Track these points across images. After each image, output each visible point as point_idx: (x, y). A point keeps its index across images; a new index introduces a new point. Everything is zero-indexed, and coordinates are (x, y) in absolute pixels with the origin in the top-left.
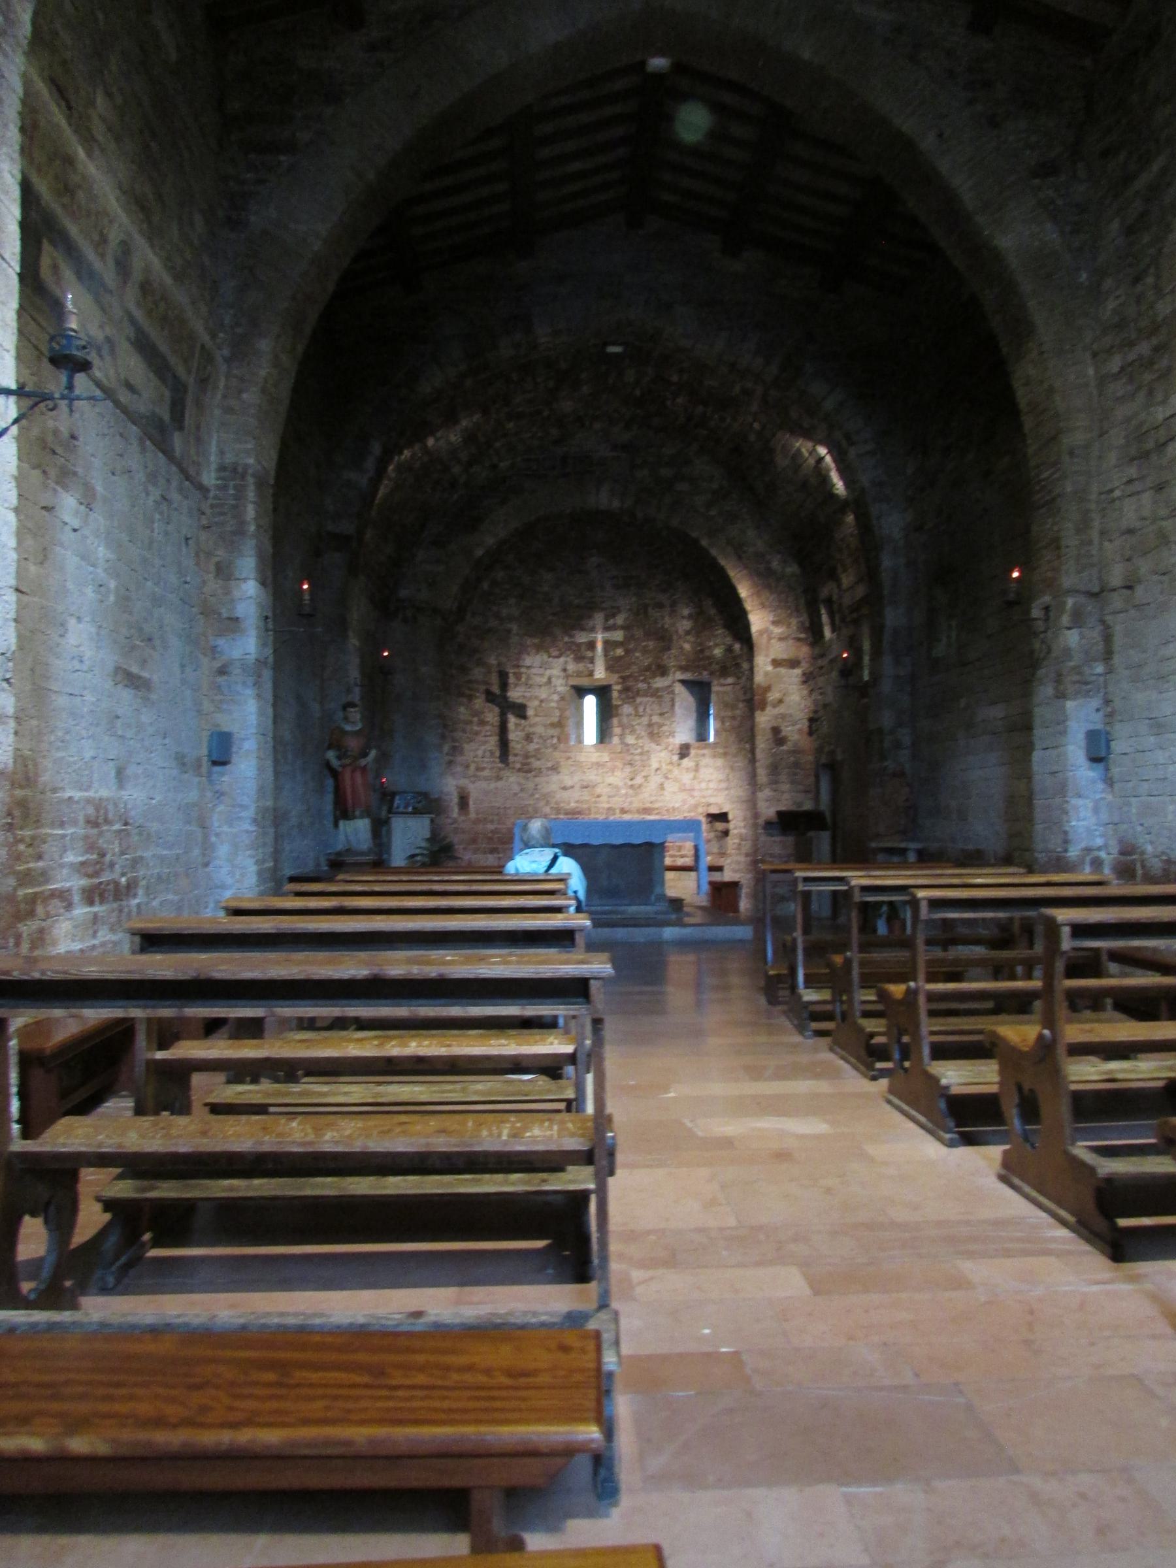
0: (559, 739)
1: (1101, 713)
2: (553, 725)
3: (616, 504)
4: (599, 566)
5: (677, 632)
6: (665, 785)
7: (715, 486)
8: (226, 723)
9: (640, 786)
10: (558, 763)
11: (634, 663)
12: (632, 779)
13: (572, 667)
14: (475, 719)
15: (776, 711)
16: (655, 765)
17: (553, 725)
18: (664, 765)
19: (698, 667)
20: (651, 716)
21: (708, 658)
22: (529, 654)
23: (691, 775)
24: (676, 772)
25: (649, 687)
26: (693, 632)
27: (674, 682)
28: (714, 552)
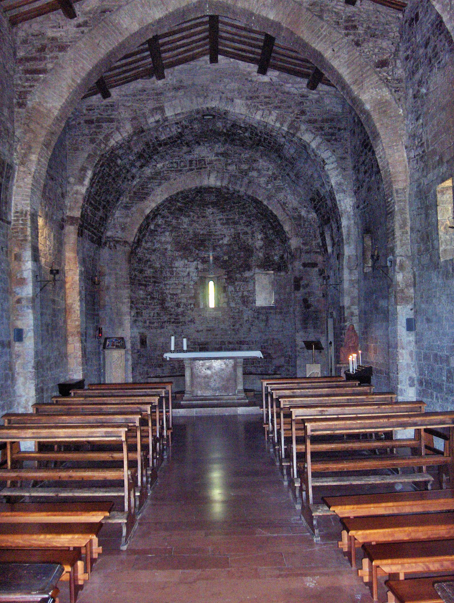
0: (194, 305)
1: (413, 311)
3: (219, 184)
4: (213, 213)
5: (255, 247)
7: (270, 173)
8: (19, 324)
13: (200, 267)
14: (149, 297)
16: (246, 318)
17: (191, 298)
22: (177, 260)
25: (242, 276)
28: (270, 208)
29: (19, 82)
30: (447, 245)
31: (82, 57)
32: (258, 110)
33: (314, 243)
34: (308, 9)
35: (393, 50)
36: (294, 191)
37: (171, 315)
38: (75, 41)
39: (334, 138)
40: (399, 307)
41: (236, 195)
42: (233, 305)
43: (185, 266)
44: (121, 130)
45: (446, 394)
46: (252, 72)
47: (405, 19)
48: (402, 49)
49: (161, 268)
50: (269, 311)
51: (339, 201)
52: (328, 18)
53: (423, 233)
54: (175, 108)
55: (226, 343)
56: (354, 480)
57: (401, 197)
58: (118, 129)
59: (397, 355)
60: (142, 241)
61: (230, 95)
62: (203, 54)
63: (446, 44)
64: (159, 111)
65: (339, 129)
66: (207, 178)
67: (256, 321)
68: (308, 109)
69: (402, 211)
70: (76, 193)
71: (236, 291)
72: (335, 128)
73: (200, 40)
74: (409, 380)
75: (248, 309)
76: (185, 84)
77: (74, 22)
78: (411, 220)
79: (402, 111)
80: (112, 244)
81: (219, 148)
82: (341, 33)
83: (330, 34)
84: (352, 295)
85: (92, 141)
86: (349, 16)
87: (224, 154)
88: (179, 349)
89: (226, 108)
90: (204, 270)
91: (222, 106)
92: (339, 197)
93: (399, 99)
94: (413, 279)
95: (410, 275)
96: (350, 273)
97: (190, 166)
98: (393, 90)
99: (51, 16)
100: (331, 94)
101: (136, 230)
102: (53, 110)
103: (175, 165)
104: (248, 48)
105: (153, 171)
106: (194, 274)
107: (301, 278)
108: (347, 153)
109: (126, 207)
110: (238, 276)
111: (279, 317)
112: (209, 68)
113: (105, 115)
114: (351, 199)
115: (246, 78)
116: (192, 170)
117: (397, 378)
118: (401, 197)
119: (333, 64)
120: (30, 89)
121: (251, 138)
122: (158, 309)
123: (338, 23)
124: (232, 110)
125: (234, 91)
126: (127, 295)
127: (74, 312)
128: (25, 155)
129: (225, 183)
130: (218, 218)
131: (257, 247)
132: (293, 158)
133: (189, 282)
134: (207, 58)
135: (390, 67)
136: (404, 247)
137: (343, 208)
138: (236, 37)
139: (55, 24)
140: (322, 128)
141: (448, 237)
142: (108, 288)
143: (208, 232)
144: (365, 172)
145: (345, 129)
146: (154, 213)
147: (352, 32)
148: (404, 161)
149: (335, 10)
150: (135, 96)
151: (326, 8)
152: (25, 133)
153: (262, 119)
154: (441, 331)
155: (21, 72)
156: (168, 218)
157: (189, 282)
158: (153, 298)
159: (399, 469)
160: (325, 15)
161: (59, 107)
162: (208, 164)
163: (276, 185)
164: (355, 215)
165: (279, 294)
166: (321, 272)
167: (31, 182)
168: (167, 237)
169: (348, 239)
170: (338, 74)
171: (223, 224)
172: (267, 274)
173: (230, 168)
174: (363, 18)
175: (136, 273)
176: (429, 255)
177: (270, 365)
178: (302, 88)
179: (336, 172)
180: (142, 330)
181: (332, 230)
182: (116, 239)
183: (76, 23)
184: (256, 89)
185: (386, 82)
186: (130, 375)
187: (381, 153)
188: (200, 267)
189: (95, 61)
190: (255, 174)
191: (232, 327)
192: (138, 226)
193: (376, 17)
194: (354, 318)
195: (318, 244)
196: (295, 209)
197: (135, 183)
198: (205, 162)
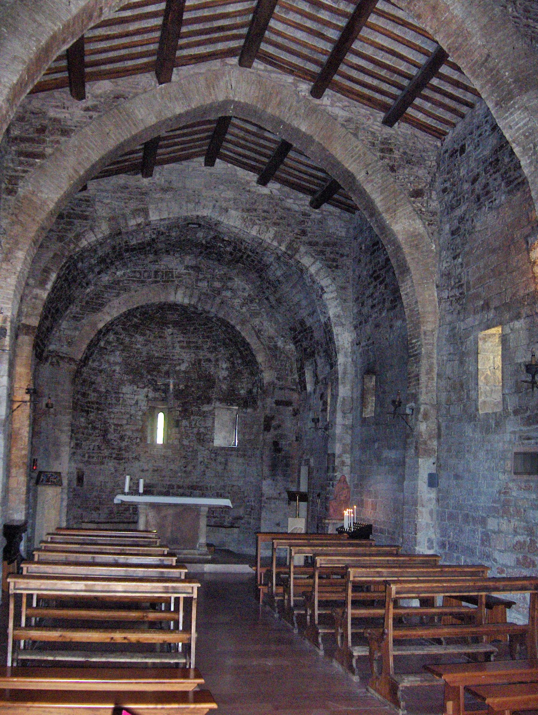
0: (141, 439)
3: (186, 301)
4: (172, 334)
6: (206, 473)
7: (246, 294)
9: (190, 472)
10: (139, 455)
12: (185, 467)
13: (151, 395)
14: (90, 426)
16: (200, 459)
17: (137, 430)
21: (236, 395)
22: (125, 386)
23: (223, 467)
24: (213, 464)
25: (200, 410)
27: (214, 408)
28: (243, 334)
29: (11, 165)
30: (487, 396)
31: (88, 147)
32: (254, 224)
34: (343, 125)
35: (429, 180)
36: (271, 317)
37: (113, 449)
38: (82, 127)
39: (335, 264)
40: (420, 460)
41: (204, 315)
42: (186, 442)
43: (134, 393)
44: (96, 230)
45: (479, 558)
46: (251, 181)
47: (444, 148)
48: (439, 180)
51: (337, 335)
52: (363, 138)
53: (455, 381)
54: (160, 211)
55: (175, 487)
56: (416, 650)
57: (429, 339)
58: (92, 229)
59: (416, 513)
60: (89, 359)
61: (224, 205)
62: (197, 155)
63: (503, 184)
64: (141, 214)
65: (342, 256)
66: (173, 293)
67: (213, 463)
68: (309, 229)
69: (429, 356)
70: (36, 298)
72: (337, 253)
73: (198, 140)
75: (204, 449)
76: (174, 187)
77: (83, 104)
78: (439, 366)
79: (434, 246)
81: (189, 260)
82: (375, 155)
83: (365, 154)
84: (344, 441)
85: (60, 239)
86: (385, 139)
87: (196, 268)
88: (134, 492)
89: (219, 219)
90: (155, 399)
91: (215, 216)
92: (336, 330)
93: (432, 234)
95: (434, 426)
96: (344, 417)
97: (156, 277)
98: (427, 223)
99: (55, 93)
100: (335, 216)
102: (48, 202)
103: (138, 275)
104: (253, 155)
105: (112, 279)
107: (273, 418)
108: (348, 282)
109: (75, 318)
110: (194, 409)
111: (240, 460)
112: (203, 171)
113: (78, 210)
114: (350, 334)
115: (243, 187)
116: (157, 282)
117: (415, 539)
118: (429, 339)
119: (365, 187)
120: (24, 175)
121: (231, 254)
122: (99, 439)
123: (373, 145)
124: (225, 221)
125: (229, 200)
128: (10, 251)
129: (194, 301)
130: (179, 339)
132: (279, 281)
134: (202, 159)
135: (425, 198)
136: (430, 394)
138: (242, 142)
139: (59, 104)
140: (322, 252)
141: (488, 388)
144: (373, 307)
145: (348, 256)
146: (107, 327)
147: (387, 155)
148: (434, 300)
149: (370, 129)
150: (115, 192)
151: (362, 127)
152: (13, 224)
153: (258, 235)
154: (475, 490)
155: (14, 153)
159: (442, 639)
160: (360, 134)
161: (56, 200)
162: (177, 277)
163: (252, 308)
164: (353, 352)
165: (244, 434)
166: (296, 413)
167: (15, 283)
168: (117, 357)
170: (369, 198)
171: (182, 347)
172: (228, 409)
173: (200, 284)
174: (400, 142)
176: (462, 406)
178: (304, 205)
179: (335, 303)
180: (81, 465)
181: (316, 366)
182: (61, 355)
183: (84, 105)
184: (253, 201)
185: (420, 213)
186: (64, 518)
187: (408, 290)
188: (151, 395)
189: (103, 153)
190: (229, 294)
191: (184, 469)
192: (88, 342)
193: (414, 143)
197: (88, 290)
198: (172, 275)
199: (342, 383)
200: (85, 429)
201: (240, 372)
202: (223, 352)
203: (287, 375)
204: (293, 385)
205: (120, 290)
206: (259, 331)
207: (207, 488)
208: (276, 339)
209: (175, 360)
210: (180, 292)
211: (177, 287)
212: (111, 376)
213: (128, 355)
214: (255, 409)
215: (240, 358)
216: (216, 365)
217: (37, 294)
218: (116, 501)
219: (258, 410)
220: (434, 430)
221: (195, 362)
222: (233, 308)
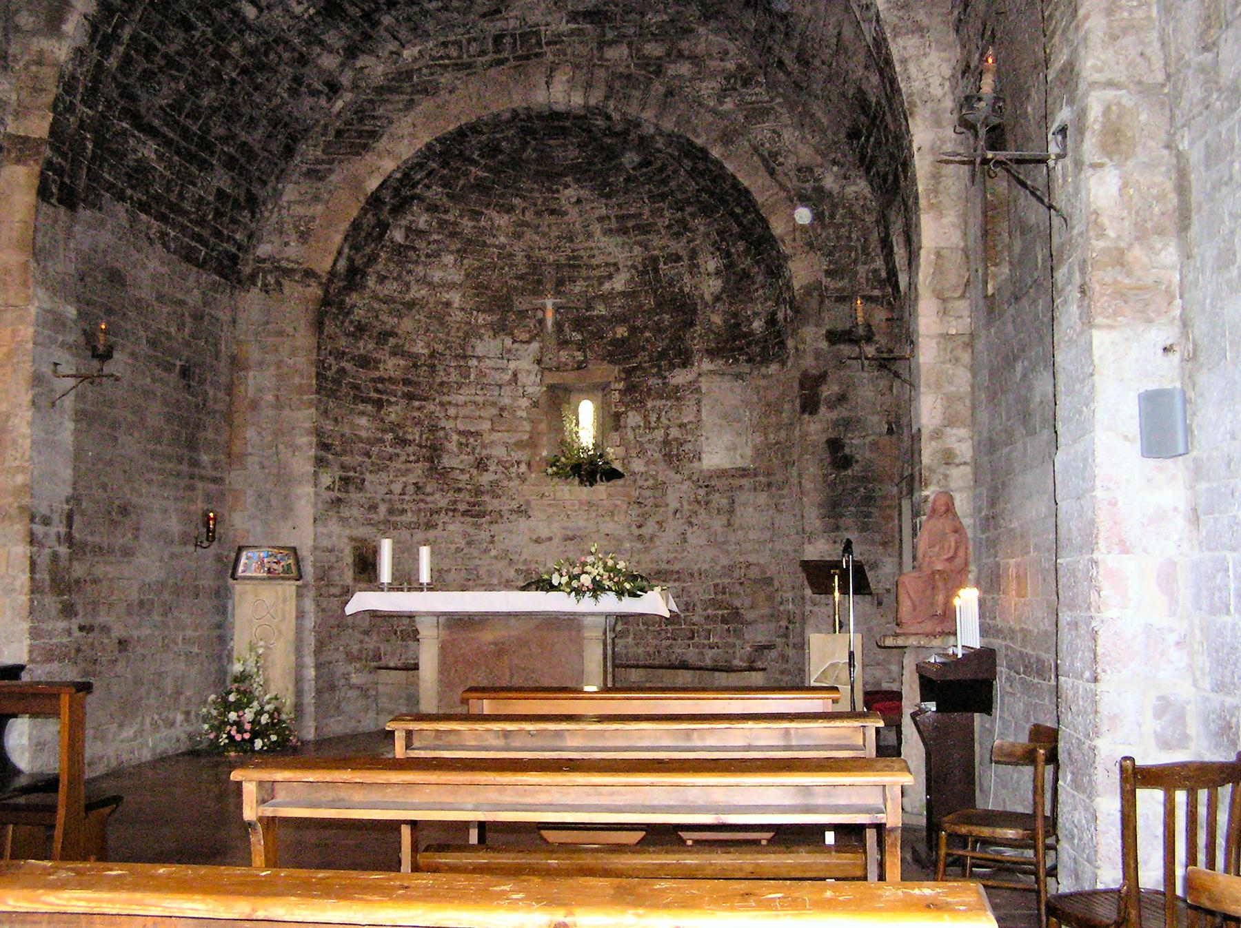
0: (529, 465)
1: (1175, 358)
2: (520, 445)
3: (577, 100)
4: (579, 201)
6: (688, 535)
7: (731, 66)
10: (528, 503)
11: (644, 349)
12: (640, 527)
14: (390, 436)
15: (834, 415)
16: (674, 504)
17: (520, 445)
18: (685, 504)
19: (733, 350)
20: (668, 427)
21: (745, 335)
22: (481, 338)
23: (725, 522)
26: (724, 296)
28: (730, 167)
33: (862, 270)
37: (460, 490)
43: (506, 354)
49: (432, 356)
50: (737, 482)
60: (364, 275)
66: (544, 86)
71: (648, 426)
74: (1158, 715)
80: (271, 279)
94: (1173, 199)
97: (497, 51)
101: (338, 238)
103: (454, 52)
106: (532, 377)
107: (822, 378)
110: (654, 382)
111: (762, 498)
116: (500, 62)
117: (1094, 699)
122: (420, 469)
126: (308, 425)
127: (14, 442)
130: (597, 214)
131: (708, 297)
133: (514, 398)
136: (1128, 40)
137: (917, 85)
142: (254, 405)
143: (569, 258)
156: (446, 212)
157: (514, 398)
158: (403, 442)
169: (936, 192)
171: (608, 232)
173: (610, 53)
175: (347, 366)
177: (738, 642)
182: (284, 264)
190: (684, 69)
191: (636, 532)
192: (345, 226)
194: (955, 472)
195: (875, 271)
196: (804, 171)
197: (339, 104)
199: (931, 206)
200: (373, 444)
201: (746, 275)
202: (702, 228)
203: (855, 262)
204: (874, 288)
205: (412, 93)
206: (774, 155)
207: (692, 575)
208: (818, 171)
209: (598, 266)
210: (561, 78)
211: (552, 70)
212: (440, 316)
213: (477, 264)
214: (784, 363)
215: (741, 237)
216: (694, 268)
217: (41, 52)
218: (350, 609)
219: (789, 364)
220: (1161, 198)
221: (645, 266)
222: (700, 104)
